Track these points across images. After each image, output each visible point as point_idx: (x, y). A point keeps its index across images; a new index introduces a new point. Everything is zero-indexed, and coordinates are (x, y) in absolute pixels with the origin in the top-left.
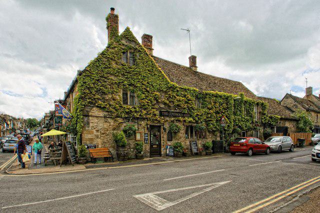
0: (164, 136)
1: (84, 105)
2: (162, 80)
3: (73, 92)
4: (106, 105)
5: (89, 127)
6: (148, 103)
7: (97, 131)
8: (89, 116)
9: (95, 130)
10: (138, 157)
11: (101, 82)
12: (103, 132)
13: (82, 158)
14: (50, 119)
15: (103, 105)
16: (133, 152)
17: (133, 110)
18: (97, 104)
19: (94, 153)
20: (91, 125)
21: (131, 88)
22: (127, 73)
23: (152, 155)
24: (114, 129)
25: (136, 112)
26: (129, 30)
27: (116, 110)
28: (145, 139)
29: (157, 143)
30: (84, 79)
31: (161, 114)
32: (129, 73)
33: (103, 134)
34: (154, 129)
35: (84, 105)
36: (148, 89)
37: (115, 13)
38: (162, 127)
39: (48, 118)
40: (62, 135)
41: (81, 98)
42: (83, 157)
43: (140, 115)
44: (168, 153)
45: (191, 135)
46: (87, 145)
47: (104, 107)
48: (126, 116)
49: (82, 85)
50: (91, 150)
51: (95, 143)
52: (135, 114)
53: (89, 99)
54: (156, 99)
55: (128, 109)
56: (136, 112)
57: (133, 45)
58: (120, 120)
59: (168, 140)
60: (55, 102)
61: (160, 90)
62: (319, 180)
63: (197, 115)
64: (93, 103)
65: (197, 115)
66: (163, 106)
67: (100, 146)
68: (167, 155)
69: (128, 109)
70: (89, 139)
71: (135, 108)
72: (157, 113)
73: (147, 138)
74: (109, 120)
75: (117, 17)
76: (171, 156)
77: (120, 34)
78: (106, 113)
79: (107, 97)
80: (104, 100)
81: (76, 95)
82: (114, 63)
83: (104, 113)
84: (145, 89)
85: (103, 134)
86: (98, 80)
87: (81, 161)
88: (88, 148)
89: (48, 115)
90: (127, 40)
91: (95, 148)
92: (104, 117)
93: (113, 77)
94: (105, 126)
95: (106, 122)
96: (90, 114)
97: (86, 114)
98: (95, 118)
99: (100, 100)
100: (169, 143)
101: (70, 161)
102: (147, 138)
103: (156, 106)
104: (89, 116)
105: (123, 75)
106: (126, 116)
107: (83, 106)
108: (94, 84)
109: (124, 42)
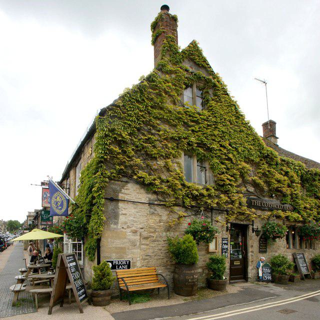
0: (253, 242)
1: (109, 178)
2: (252, 142)
3: (76, 166)
4: (154, 180)
5: (116, 223)
6: (230, 180)
7: (135, 232)
8: (118, 200)
9: (129, 230)
10: (213, 283)
11: (143, 134)
12: (145, 234)
13: (102, 292)
14: (35, 219)
15: (148, 179)
16: (201, 274)
17: (205, 192)
18: (135, 177)
19: (131, 280)
20: (122, 219)
21: (201, 150)
22: (193, 121)
23: (232, 281)
24: (169, 229)
25: (210, 196)
26: (196, 45)
27: (174, 190)
28: (222, 249)
29: (240, 257)
30: (110, 123)
31: (250, 205)
32: (197, 122)
33: (146, 238)
34: (239, 231)
35: (109, 178)
36: (231, 156)
37: (172, 12)
38: (251, 227)
39: (32, 218)
40: (52, 240)
41: (101, 162)
42: (104, 289)
43: (217, 203)
44: (260, 275)
45: (293, 245)
46: (112, 262)
47: (151, 184)
48: (193, 203)
49: (106, 136)
50: (121, 273)
51: (128, 257)
52: (209, 201)
53: (119, 165)
54: (242, 176)
55: (197, 190)
56: (210, 196)
57: (202, 73)
58: (180, 211)
59: (260, 252)
60: (43, 184)
61: (249, 161)
62: (318, 294)
63: (305, 208)
64: (127, 174)
65: (305, 208)
66: (252, 189)
67: (138, 264)
68: (259, 279)
69: (197, 190)
70: (116, 248)
71: (208, 190)
72: (244, 200)
73: (225, 247)
74: (159, 210)
75: (174, 19)
76: (268, 281)
77: (180, 51)
78: (153, 197)
79: (156, 165)
80: (150, 170)
81: (91, 156)
82: (93, 189)
83: (150, 196)
84: (225, 154)
85: (146, 238)
86: (139, 130)
87: (100, 299)
88: (114, 267)
89: (32, 214)
90: (192, 63)
91: (129, 267)
92: (149, 204)
93: (167, 127)
94: (151, 222)
95: (153, 213)
96: (121, 196)
97: (112, 195)
98: (131, 205)
99: (142, 169)
100: (263, 257)
101: (73, 296)
102: (225, 247)
103: (243, 189)
104: (118, 200)
105: (186, 125)
106: (193, 203)
107: (107, 180)
108: (130, 135)
109: (187, 65)
